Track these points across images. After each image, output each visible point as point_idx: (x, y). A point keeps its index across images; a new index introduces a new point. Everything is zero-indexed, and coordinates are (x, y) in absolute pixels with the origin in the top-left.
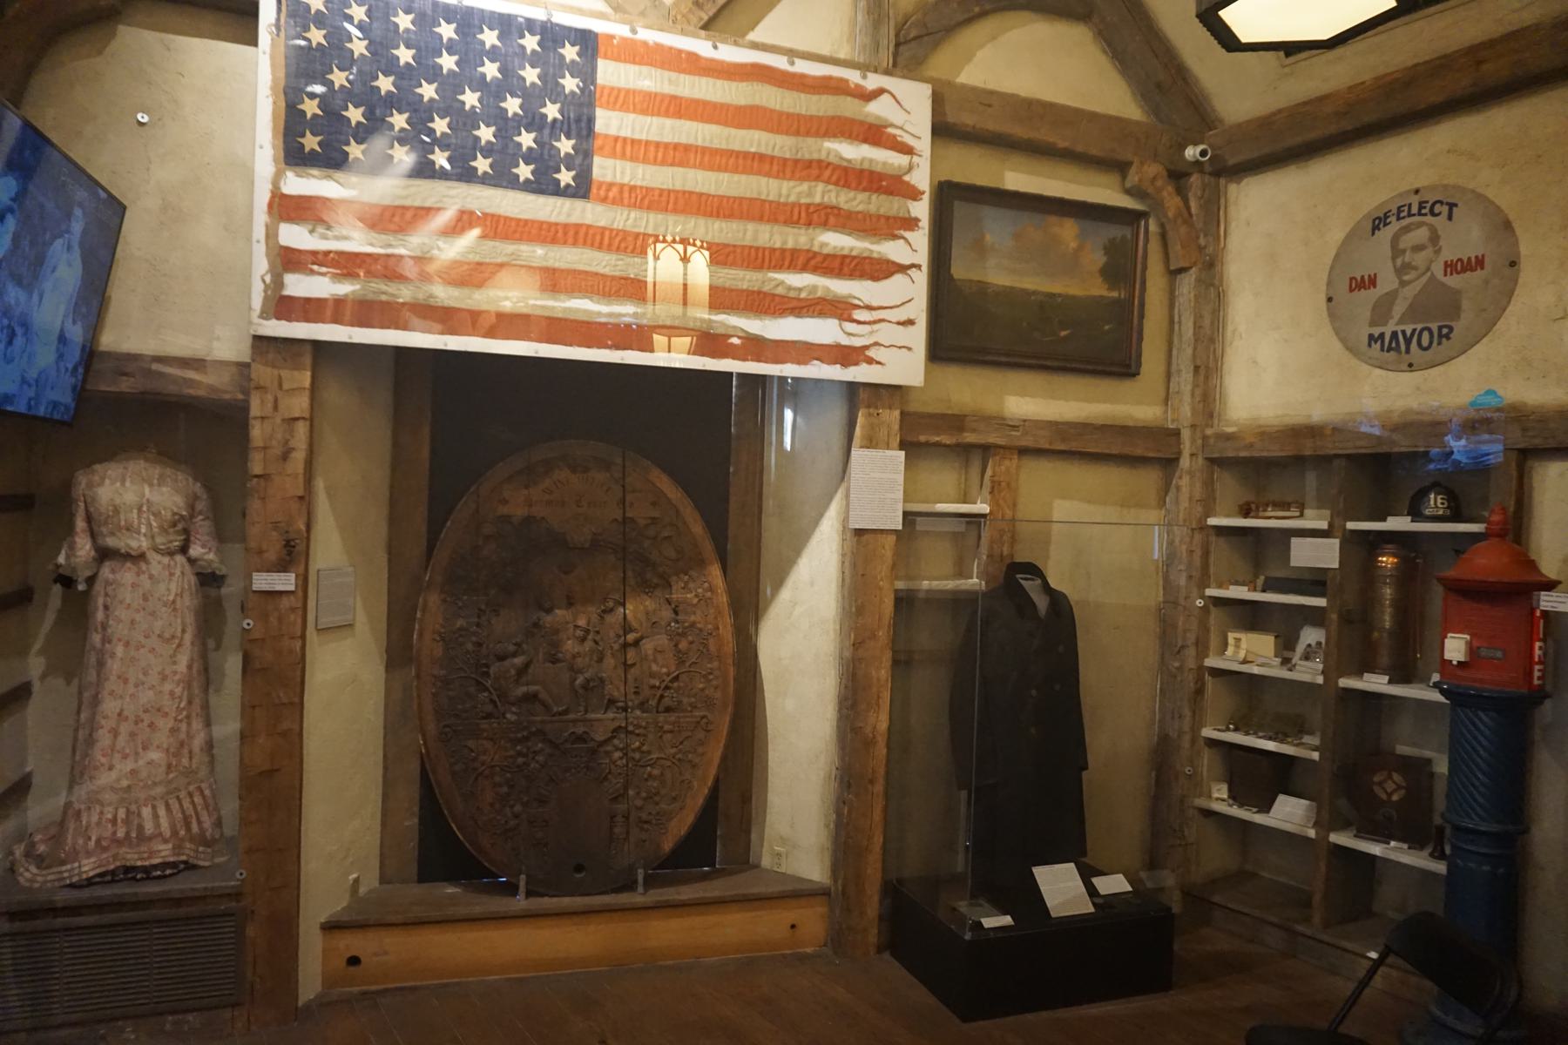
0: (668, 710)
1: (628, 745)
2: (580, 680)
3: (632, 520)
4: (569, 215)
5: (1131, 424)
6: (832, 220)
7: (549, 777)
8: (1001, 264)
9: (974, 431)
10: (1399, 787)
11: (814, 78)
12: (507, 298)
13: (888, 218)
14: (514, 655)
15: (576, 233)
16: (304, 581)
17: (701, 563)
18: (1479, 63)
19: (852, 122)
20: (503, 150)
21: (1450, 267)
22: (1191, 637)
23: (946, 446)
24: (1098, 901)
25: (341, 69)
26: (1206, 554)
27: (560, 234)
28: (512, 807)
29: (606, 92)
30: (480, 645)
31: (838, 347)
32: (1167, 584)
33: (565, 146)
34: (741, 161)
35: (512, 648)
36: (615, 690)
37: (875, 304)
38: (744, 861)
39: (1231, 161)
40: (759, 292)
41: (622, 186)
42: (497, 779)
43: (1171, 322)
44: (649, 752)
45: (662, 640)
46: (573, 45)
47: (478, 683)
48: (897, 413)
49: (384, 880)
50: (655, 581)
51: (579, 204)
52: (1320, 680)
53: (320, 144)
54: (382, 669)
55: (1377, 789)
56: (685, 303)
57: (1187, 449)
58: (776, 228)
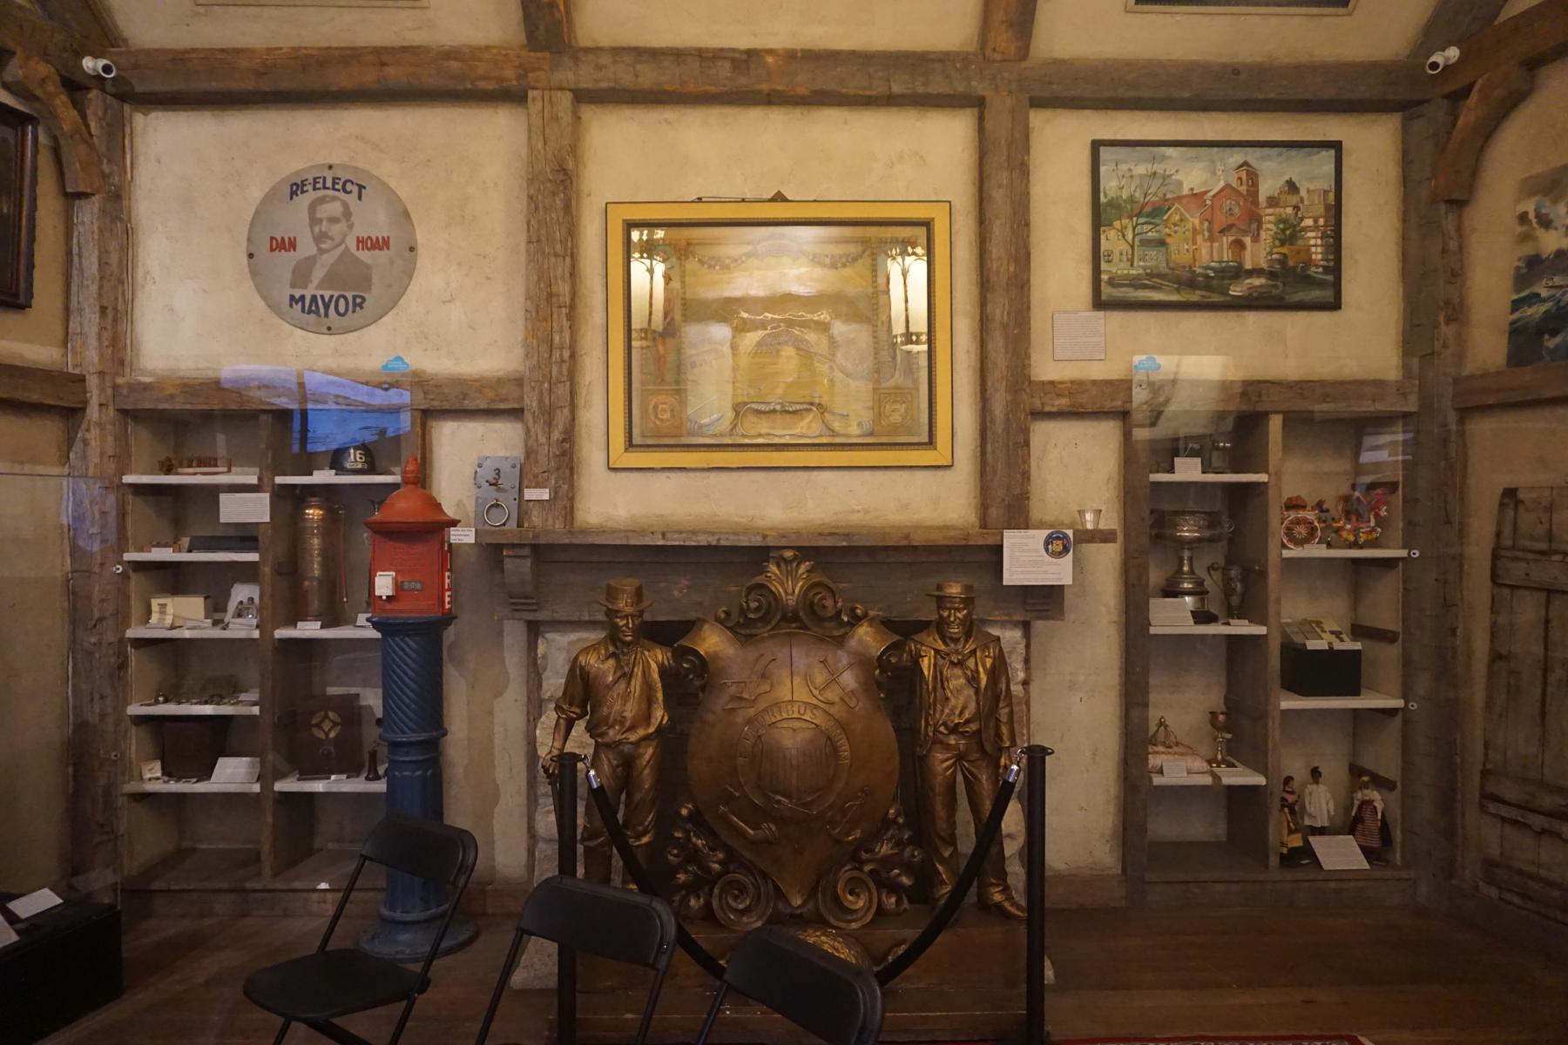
10: (335, 724)
21: (362, 243)
24: (20, 926)
26: (122, 515)
43: (69, 253)
52: (256, 634)
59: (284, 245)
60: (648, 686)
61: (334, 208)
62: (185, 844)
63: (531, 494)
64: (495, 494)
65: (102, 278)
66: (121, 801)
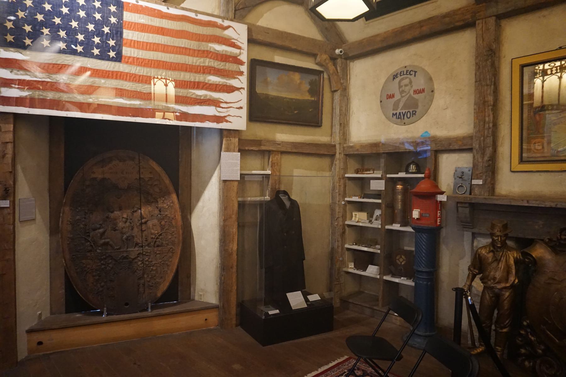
0: (158, 246)
1: (143, 259)
2: (125, 237)
3: (143, 178)
4: (114, 68)
5: (320, 143)
6: (212, 72)
7: (114, 270)
8: (273, 88)
9: (264, 145)
10: (404, 260)
11: (205, 21)
12: (91, 98)
13: (232, 71)
14: (99, 229)
15: (117, 74)
16: (13, 203)
17: (169, 193)
18: (421, 27)
19: (219, 37)
20: (87, 44)
21: (415, 92)
22: (341, 215)
23: (255, 151)
24: (309, 303)
25: (22, 11)
26: (345, 186)
27: (110, 75)
28: (100, 283)
29: (127, 23)
30: (86, 225)
31: (215, 116)
32: (333, 198)
33: (112, 43)
34: (181, 50)
35: (98, 226)
36: (138, 240)
37: (228, 101)
38: (189, 298)
39: (350, 55)
40: (186, 97)
41: (134, 58)
42: (94, 274)
43: (333, 109)
44: (151, 261)
45: (155, 221)
46: (114, 6)
47: (86, 239)
48: (237, 139)
49: (52, 313)
50: (152, 200)
51: (117, 64)
52: (380, 227)
53: (13, 39)
54: (47, 235)
55: (397, 261)
56: (166, 101)
57: (338, 151)
58: (192, 74)
59: (391, 96)
60: (508, 267)
61: (406, 81)
62: (361, 290)
63: (475, 182)
64: (461, 182)
65: (340, 115)
66: (342, 273)
